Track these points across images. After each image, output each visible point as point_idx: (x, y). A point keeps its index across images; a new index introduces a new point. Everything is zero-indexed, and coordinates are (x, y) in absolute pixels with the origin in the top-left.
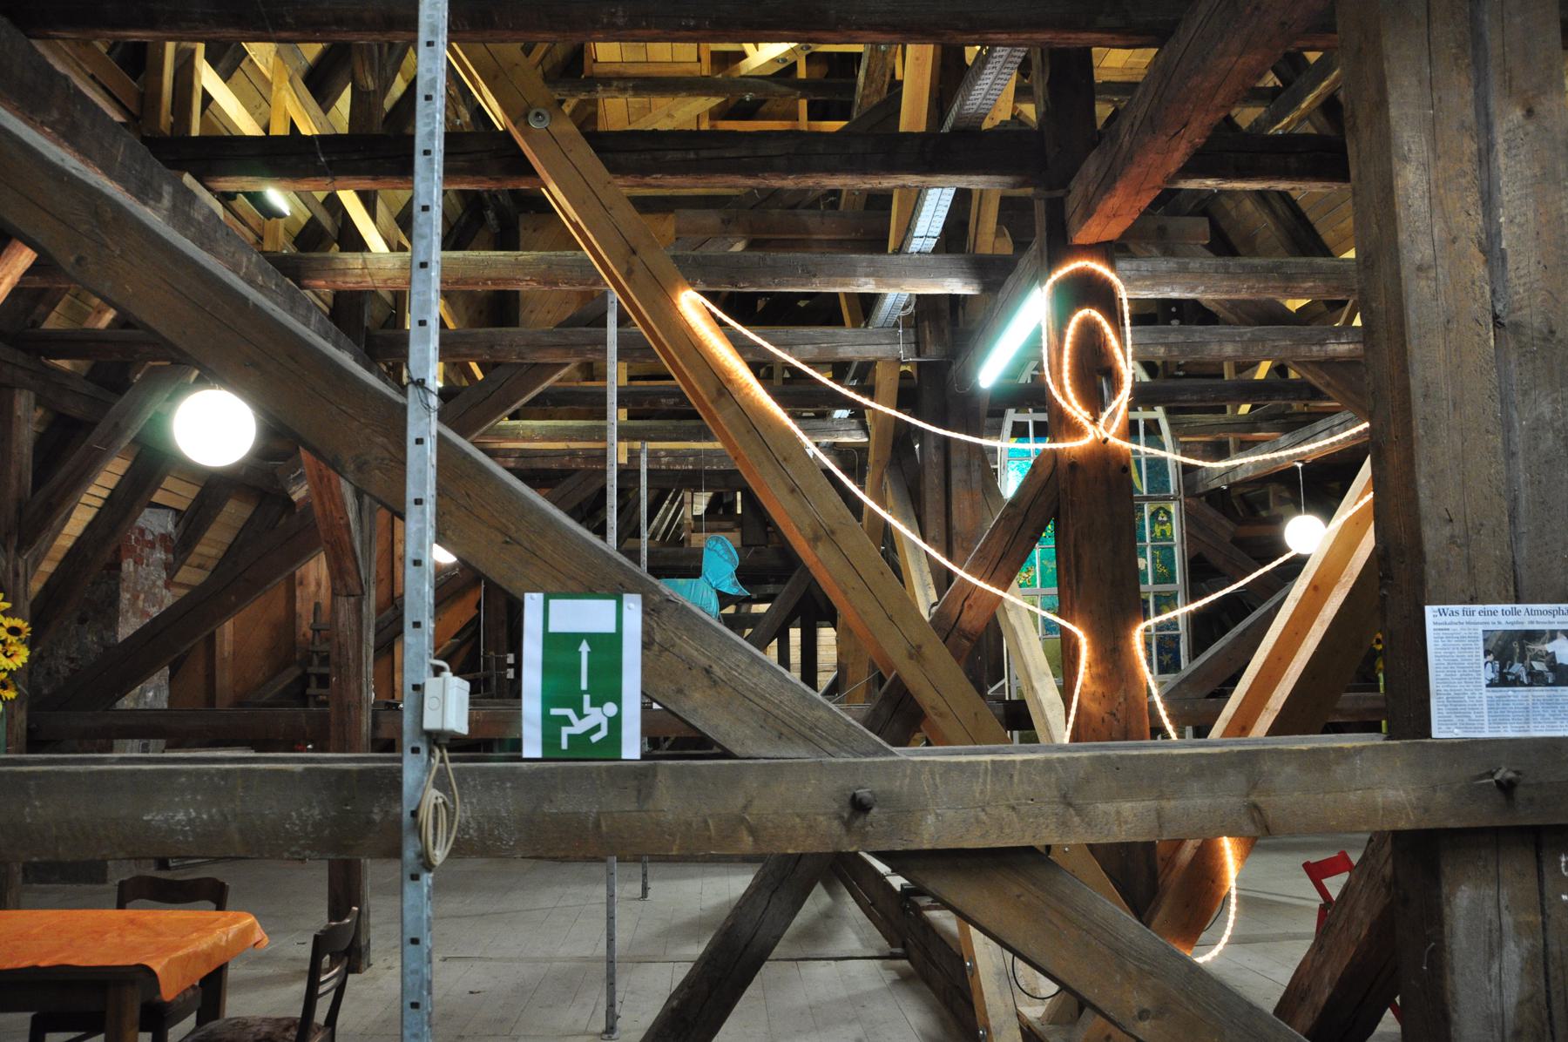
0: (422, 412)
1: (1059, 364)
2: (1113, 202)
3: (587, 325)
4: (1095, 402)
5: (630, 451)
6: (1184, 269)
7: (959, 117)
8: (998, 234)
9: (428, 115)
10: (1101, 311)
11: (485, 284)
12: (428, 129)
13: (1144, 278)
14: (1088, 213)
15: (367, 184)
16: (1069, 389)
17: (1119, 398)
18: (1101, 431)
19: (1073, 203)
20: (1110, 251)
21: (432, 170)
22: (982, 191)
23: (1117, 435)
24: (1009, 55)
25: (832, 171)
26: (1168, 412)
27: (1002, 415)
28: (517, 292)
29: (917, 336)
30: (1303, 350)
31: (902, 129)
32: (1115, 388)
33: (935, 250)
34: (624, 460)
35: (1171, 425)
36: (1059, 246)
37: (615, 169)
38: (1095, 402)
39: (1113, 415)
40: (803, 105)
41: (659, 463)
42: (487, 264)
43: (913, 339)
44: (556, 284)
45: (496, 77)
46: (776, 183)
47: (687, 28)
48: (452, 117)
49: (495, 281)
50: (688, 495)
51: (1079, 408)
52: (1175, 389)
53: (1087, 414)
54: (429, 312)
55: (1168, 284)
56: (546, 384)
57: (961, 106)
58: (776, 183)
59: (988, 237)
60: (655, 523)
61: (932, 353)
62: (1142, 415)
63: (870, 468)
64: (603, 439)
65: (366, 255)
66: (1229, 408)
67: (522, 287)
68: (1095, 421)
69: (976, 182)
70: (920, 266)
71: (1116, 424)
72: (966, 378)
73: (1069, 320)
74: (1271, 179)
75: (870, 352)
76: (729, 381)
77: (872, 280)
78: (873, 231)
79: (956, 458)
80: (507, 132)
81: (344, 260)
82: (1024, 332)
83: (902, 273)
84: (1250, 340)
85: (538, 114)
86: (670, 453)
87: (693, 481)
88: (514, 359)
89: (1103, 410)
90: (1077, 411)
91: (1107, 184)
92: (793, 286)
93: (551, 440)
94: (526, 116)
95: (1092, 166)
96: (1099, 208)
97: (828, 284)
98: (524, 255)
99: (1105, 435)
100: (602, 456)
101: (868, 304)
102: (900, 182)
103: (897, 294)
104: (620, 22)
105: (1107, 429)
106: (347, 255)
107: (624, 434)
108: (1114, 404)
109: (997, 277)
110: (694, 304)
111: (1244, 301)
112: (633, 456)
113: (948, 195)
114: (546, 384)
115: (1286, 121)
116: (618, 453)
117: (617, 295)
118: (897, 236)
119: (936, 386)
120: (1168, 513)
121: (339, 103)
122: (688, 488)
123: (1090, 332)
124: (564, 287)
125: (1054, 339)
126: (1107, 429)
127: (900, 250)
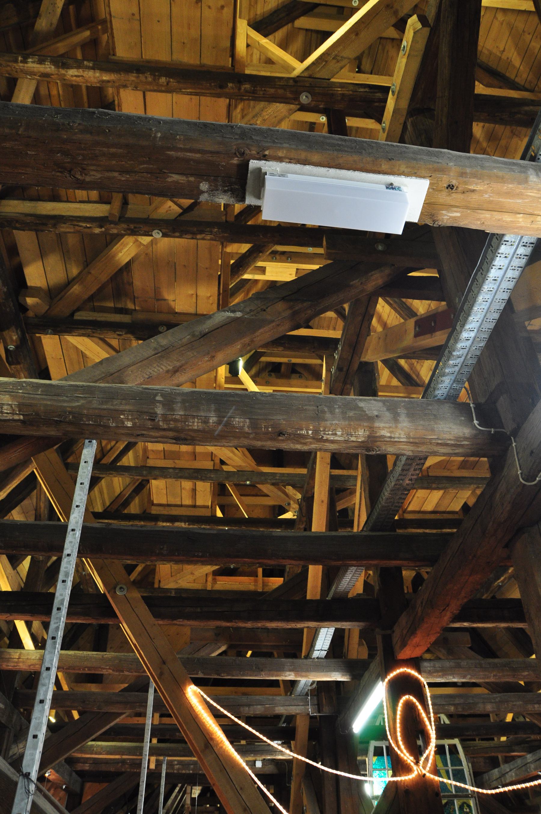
0: (24, 796)
1: (395, 728)
2: (415, 640)
3: (137, 691)
4: (417, 752)
5: (157, 761)
6: (458, 666)
7: (335, 593)
8: (360, 644)
9: (57, 618)
10: (415, 697)
11: (84, 670)
12: (56, 625)
13: (437, 671)
14: (404, 645)
15: (29, 618)
16: (402, 747)
17: (429, 748)
18: (422, 768)
19: (396, 638)
20: (415, 663)
21: (55, 648)
22: (349, 629)
23: (429, 772)
24: (356, 571)
25: (271, 620)
26: (462, 741)
27: (368, 743)
28: (103, 674)
29: (318, 701)
30: (530, 707)
31: (308, 597)
32: (427, 742)
33: (327, 657)
34: (153, 766)
35: (464, 748)
36: (391, 662)
37: (157, 615)
38: (417, 752)
39: (427, 759)
40: (260, 570)
41: (173, 769)
42: (87, 659)
43: (316, 702)
44: (123, 671)
45: (102, 568)
46: (241, 625)
47: (198, 556)
48: (80, 569)
49: (89, 668)
50: (189, 788)
51: (408, 755)
52: (463, 725)
53: (412, 758)
54: (40, 730)
55: (451, 675)
56: (112, 724)
57: (336, 588)
58: (241, 625)
59: (356, 650)
60: (170, 802)
61: (327, 711)
62: (447, 742)
63: (293, 778)
64: (141, 754)
65: (22, 651)
66: (496, 739)
67: (104, 672)
68: (417, 763)
69: (345, 625)
70: (319, 665)
71: (429, 765)
72: (347, 725)
73: (398, 702)
74: (496, 622)
75: (293, 710)
76: (212, 739)
77: (292, 673)
78: (294, 648)
79: (342, 786)
80: (104, 594)
81: (9, 653)
82: (374, 706)
83: (308, 670)
84: (500, 702)
85: (121, 588)
86: (180, 762)
87: (192, 779)
88: (95, 709)
89: (421, 755)
90: (407, 757)
91: (412, 631)
92: (251, 676)
93: (111, 754)
94: (115, 588)
95: (403, 620)
96: (409, 642)
97: (269, 675)
98: (108, 655)
99: (424, 772)
100: (138, 764)
101: (293, 683)
102: (306, 625)
103: (306, 680)
104: (165, 552)
105: (424, 768)
106: (11, 651)
107: (153, 751)
108: (427, 752)
109: (361, 675)
110: (195, 693)
111: (493, 683)
112: (159, 764)
113: (332, 631)
114: (112, 724)
115: (502, 578)
116: (148, 762)
117: (154, 685)
118: (307, 645)
119: (329, 736)
120: (469, 806)
121: (24, 562)
122: (189, 784)
123: (409, 708)
124: (126, 673)
125: (391, 713)
126: (424, 768)
127: (308, 656)
